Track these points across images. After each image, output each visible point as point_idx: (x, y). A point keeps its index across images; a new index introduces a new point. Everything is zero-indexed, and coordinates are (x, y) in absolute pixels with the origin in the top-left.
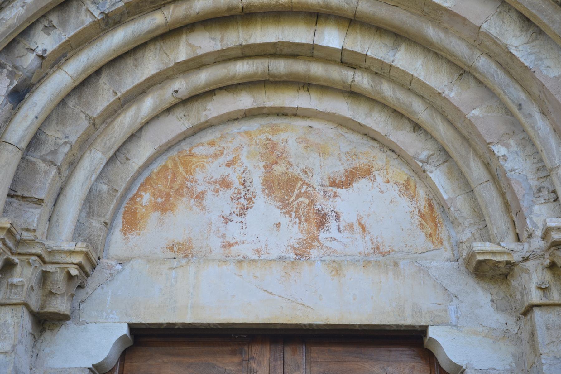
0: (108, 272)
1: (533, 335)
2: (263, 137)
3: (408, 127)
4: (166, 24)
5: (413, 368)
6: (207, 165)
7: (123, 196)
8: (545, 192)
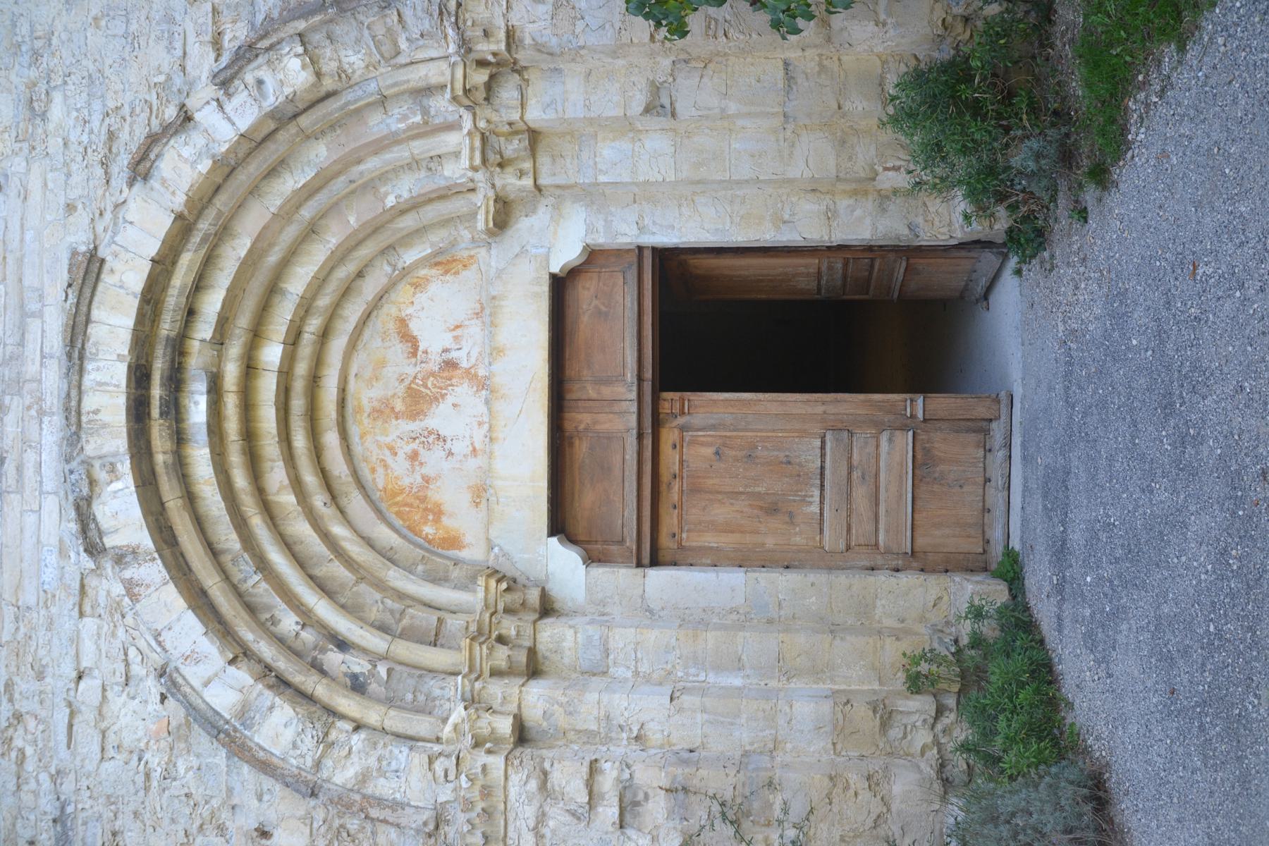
0: (500, 559)
1: (558, 187)
2: (366, 421)
3: (359, 282)
4: (261, 514)
5: (584, 288)
6: (396, 474)
7: (427, 550)
8: (432, 165)
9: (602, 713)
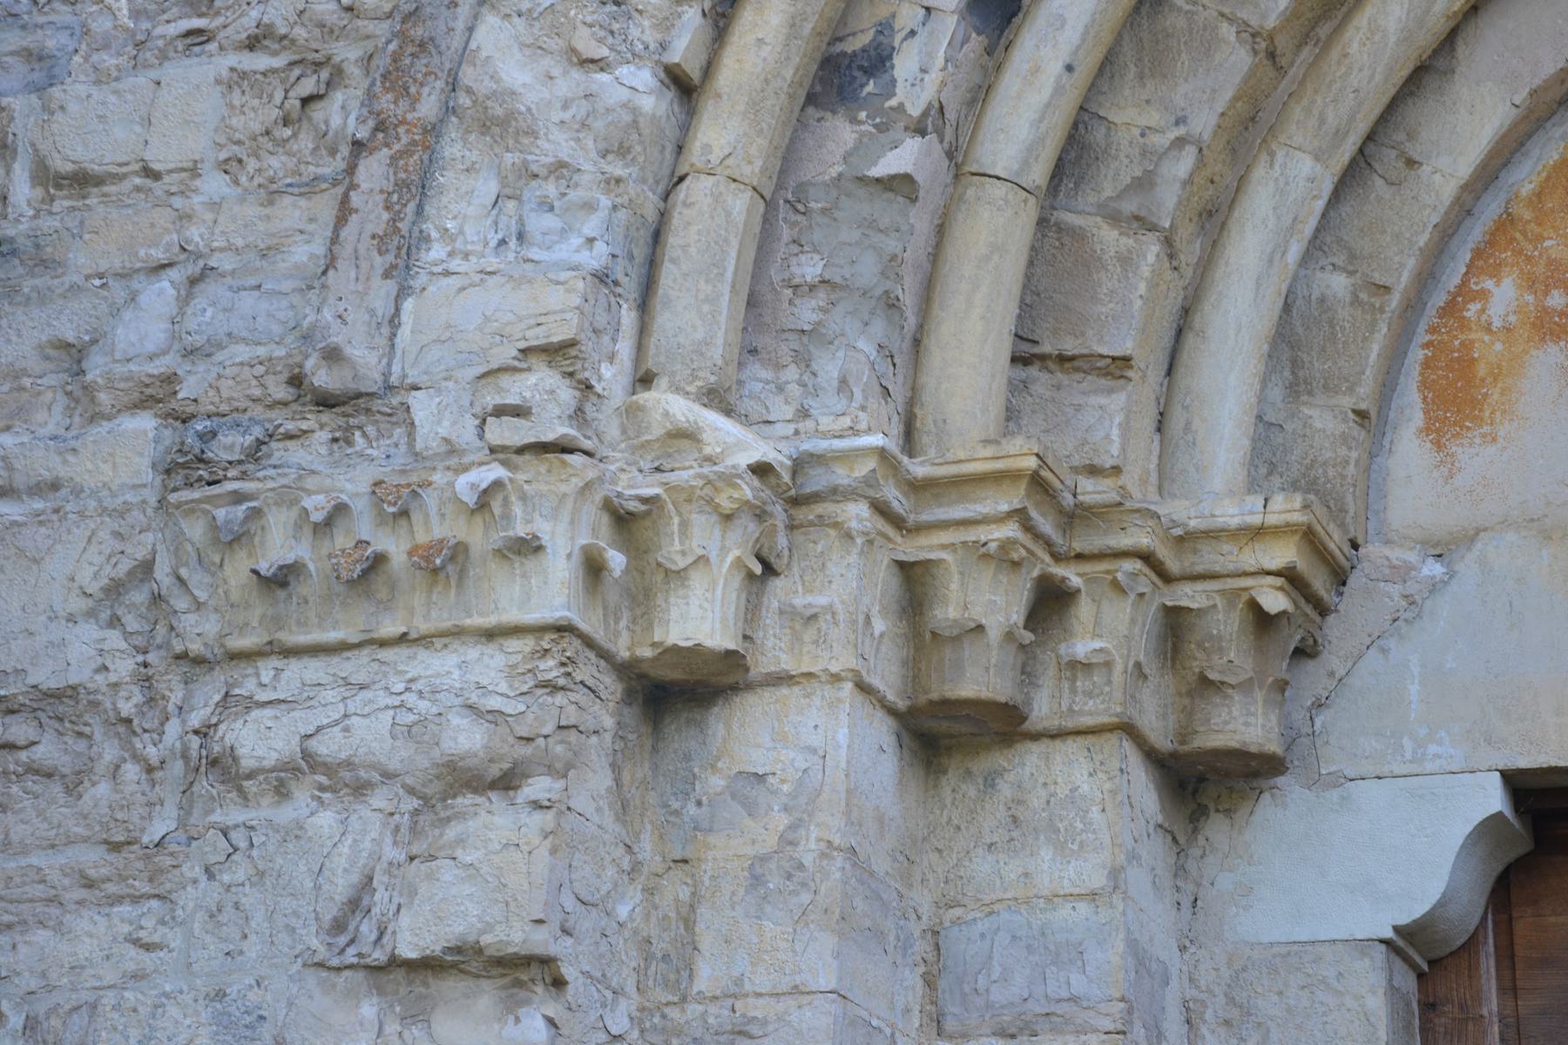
0: (1395, 590)
7: (1413, 305)
9: (757, 1008)
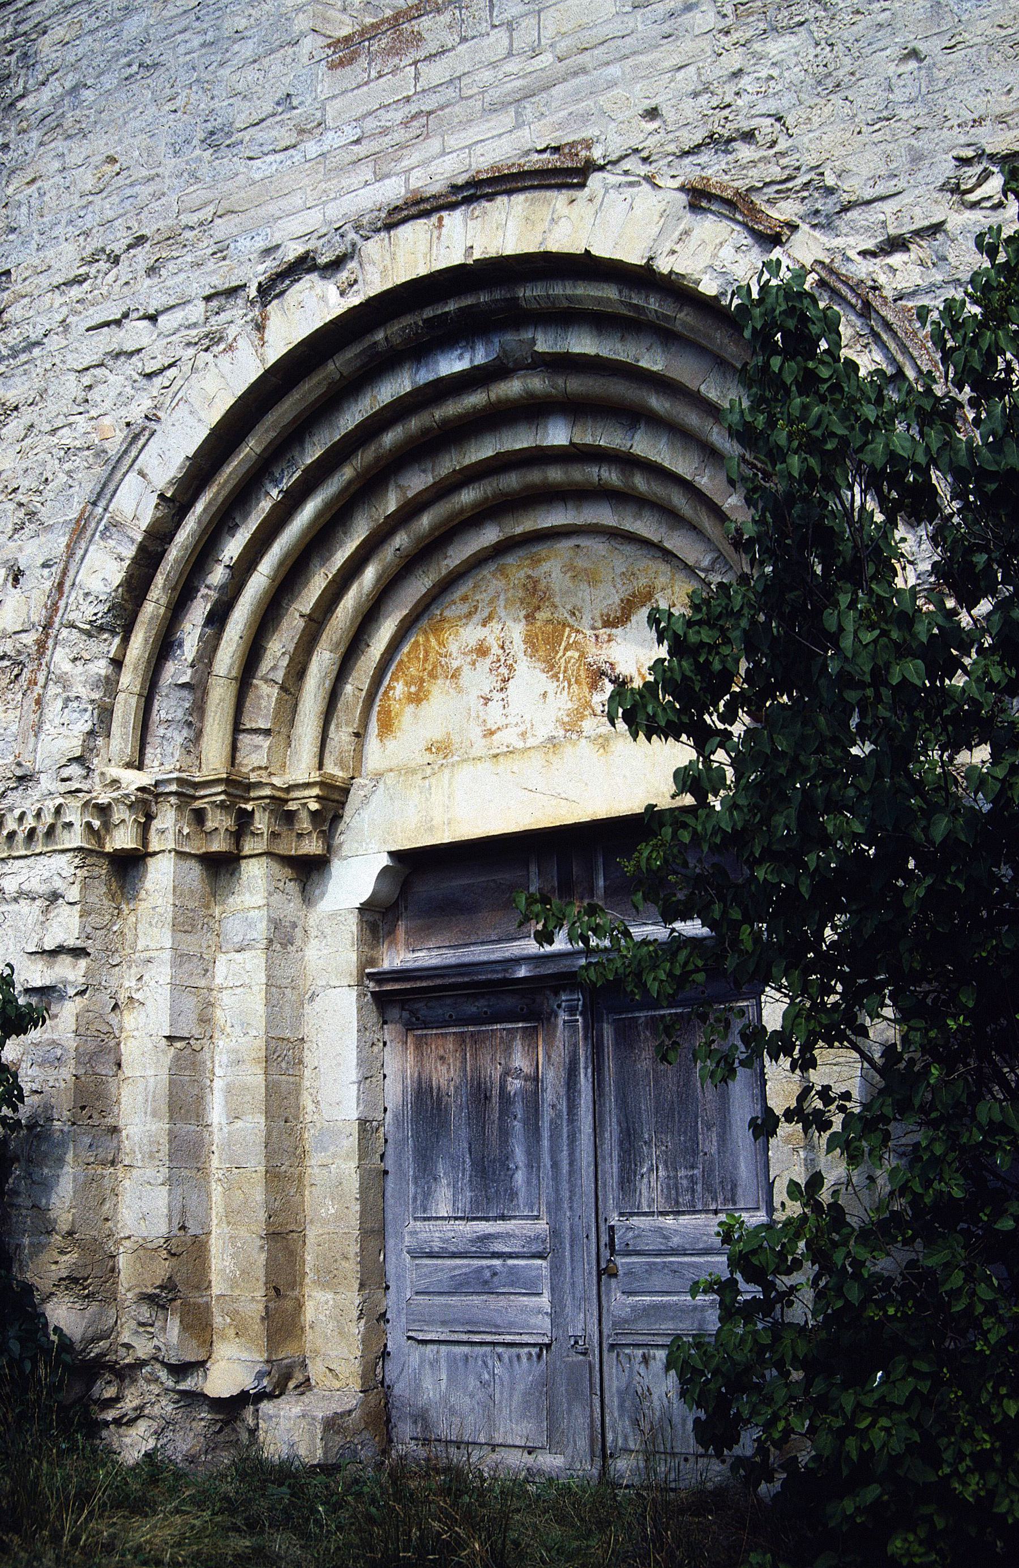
2: (522, 574)
